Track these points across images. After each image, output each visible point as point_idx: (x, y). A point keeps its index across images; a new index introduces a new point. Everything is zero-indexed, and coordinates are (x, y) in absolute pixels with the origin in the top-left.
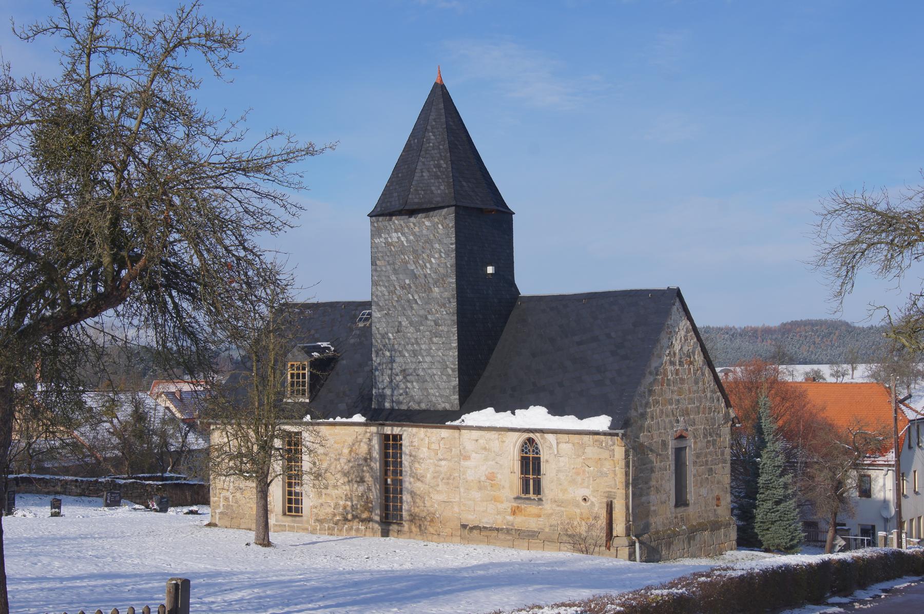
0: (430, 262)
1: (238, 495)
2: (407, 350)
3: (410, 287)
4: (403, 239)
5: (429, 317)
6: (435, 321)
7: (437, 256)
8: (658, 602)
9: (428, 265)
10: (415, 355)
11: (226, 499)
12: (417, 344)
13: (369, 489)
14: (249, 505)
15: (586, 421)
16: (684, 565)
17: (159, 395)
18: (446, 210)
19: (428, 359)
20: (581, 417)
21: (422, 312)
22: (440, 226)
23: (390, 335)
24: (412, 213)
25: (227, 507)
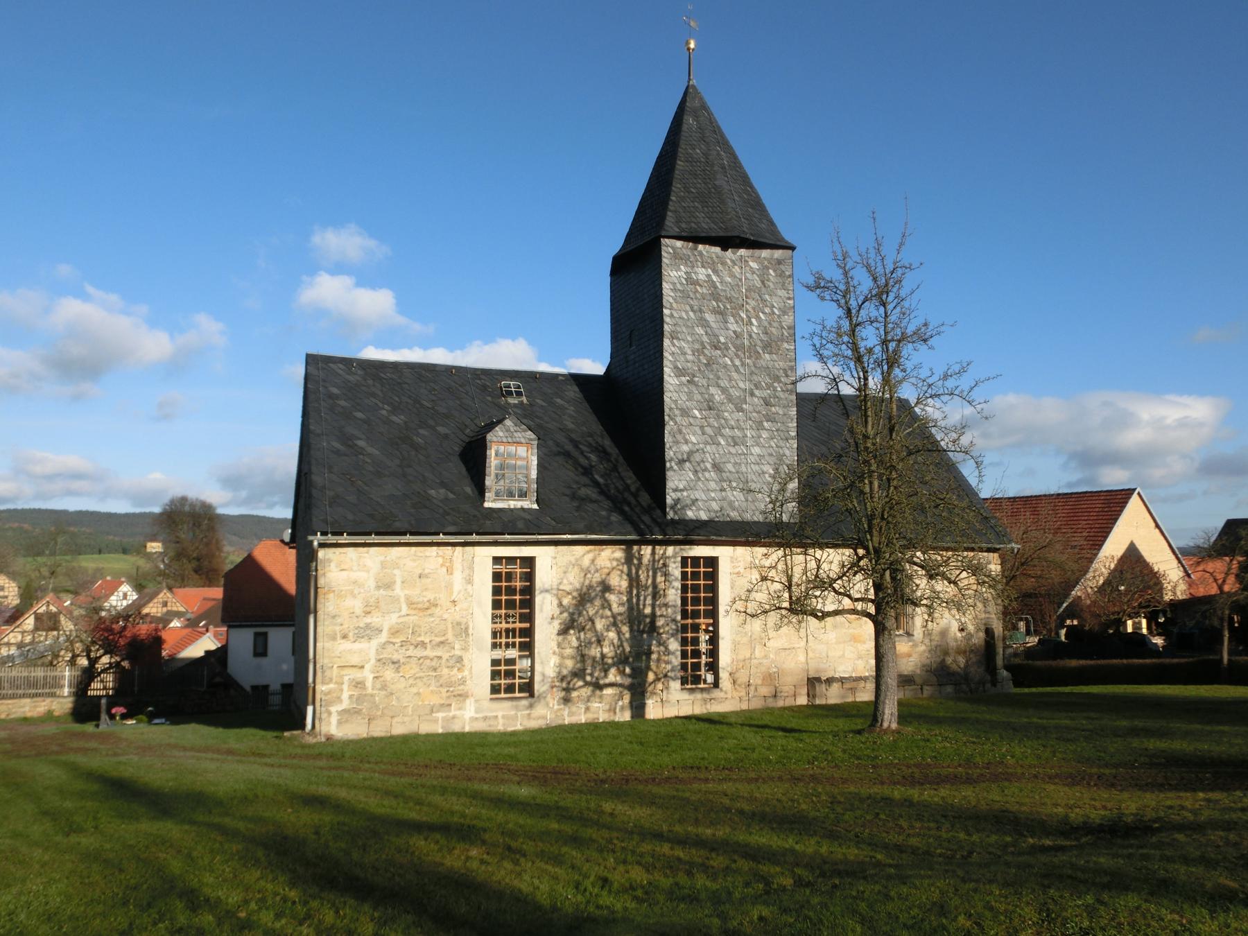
0: (758, 318)
1: (389, 674)
2: (722, 435)
3: (727, 349)
4: (714, 278)
5: (757, 392)
6: (764, 399)
7: (767, 310)
8: (613, 912)
9: (754, 321)
10: (736, 444)
11: (359, 684)
12: (740, 428)
13: (909, 655)
14: (414, 690)
15: (429, 352)
16: (1072, 719)
17: (1021, 619)
18: (780, 251)
19: (756, 450)
20: (425, 349)
21: (748, 385)
22: (771, 271)
23: (696, 412)
24: (727, 242)
25: (359, 699)
